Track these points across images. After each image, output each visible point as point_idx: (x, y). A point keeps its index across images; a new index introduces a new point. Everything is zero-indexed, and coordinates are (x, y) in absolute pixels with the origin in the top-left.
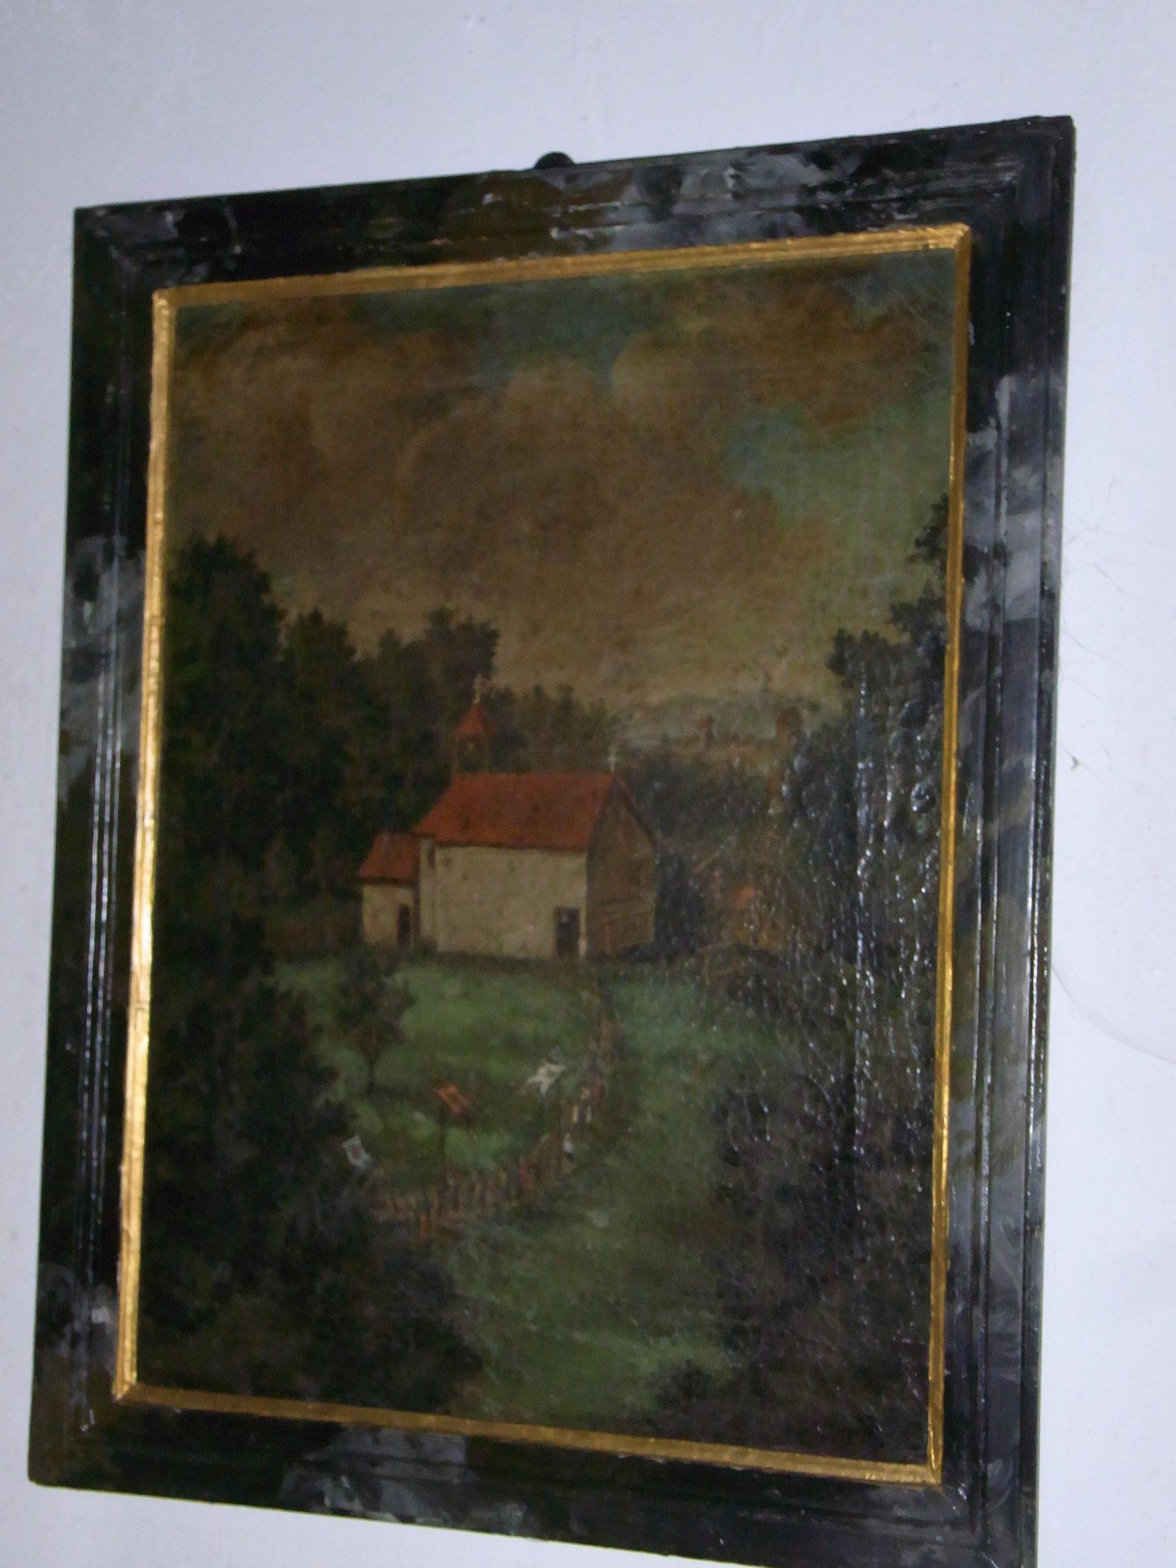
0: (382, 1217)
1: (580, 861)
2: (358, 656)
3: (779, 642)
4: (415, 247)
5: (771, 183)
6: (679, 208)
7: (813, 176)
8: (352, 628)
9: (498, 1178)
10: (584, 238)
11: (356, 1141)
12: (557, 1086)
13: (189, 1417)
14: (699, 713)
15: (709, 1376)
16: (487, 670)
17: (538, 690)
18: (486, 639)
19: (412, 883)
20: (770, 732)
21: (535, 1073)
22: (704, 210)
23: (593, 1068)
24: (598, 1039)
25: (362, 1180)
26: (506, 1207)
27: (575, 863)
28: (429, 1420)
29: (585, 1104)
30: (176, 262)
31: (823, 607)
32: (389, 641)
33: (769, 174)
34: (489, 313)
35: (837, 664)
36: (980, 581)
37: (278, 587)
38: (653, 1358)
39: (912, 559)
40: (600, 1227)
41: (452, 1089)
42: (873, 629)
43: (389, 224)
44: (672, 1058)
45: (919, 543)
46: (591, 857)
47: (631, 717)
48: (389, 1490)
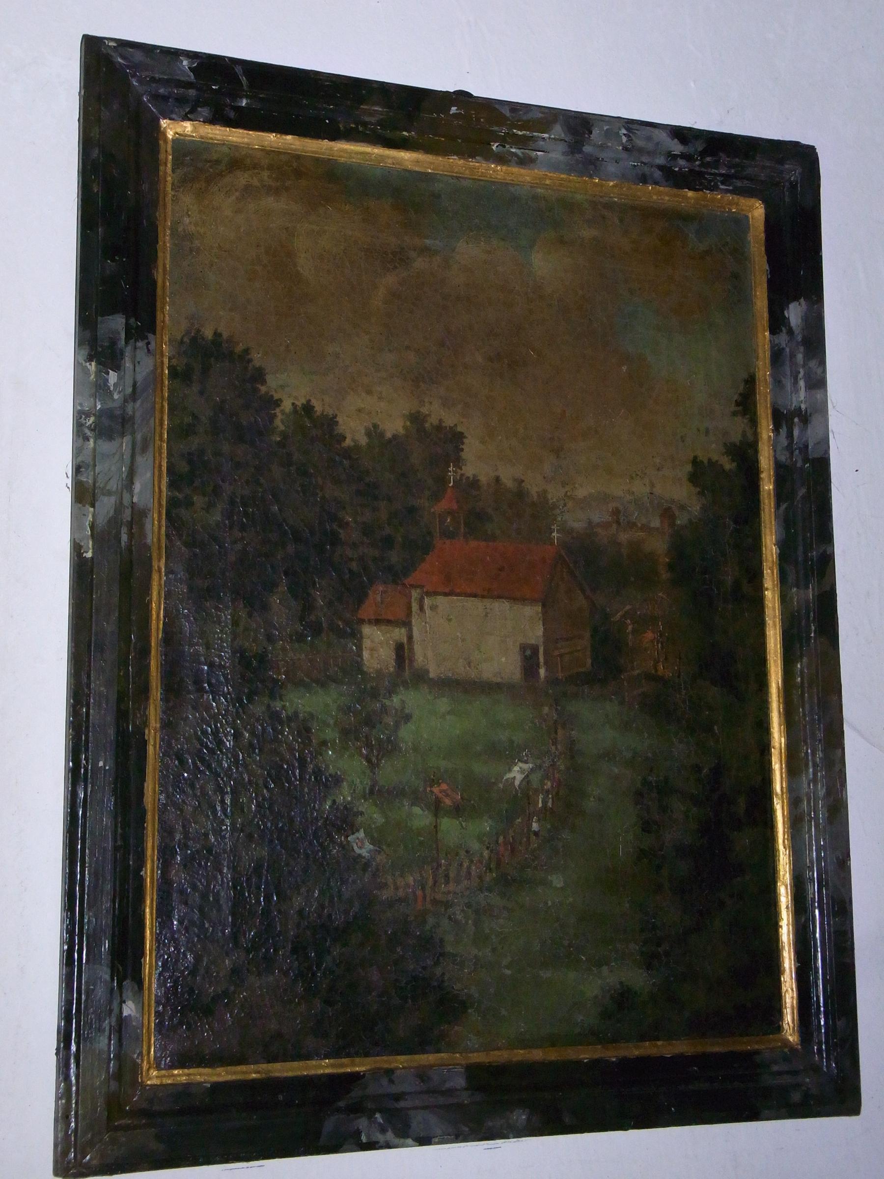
0: (385, 895)
1: (539, 609)
2: (348, 442)
3: (657, 460)
4: (388, 133)
5: (650, 146)
6: (587, 149)
7: (677, 148)
8: (339, 419)
9: (481, 855)
10: (515, 154)
11: (361, 834)
12: (527, 779)
13: (217, 1087)
14: (611, 506)
15: (636, 993)
16: (458, 462)
17: (497, 479)
18: (457, 438)
19: (407, 624)
20: (656, 523)
21: (510, 770)
22: (602, 155)
23: (553, 765)
24: (555, 743)
25: (366, 866)
26: (488, 878)
27: (531, 611)
28: (429, 1058)
29: (548, 792)
30: (181, 101)
31: (683, 439)
32: (374, 432)
33: (649, 139)
34: (437, 196)
35: (694, 478)
36: (783, 431)
37: (272, 383)
38: (593, 985)
39: (734, 414)
40: (558, 888)
41: (444, 786)
42: (715, 457)
43: (375, 112)
44: (608, 755)
45: (738, 404)
46: (544, 606)
47: (565, 505)
48: (418, 1120)
